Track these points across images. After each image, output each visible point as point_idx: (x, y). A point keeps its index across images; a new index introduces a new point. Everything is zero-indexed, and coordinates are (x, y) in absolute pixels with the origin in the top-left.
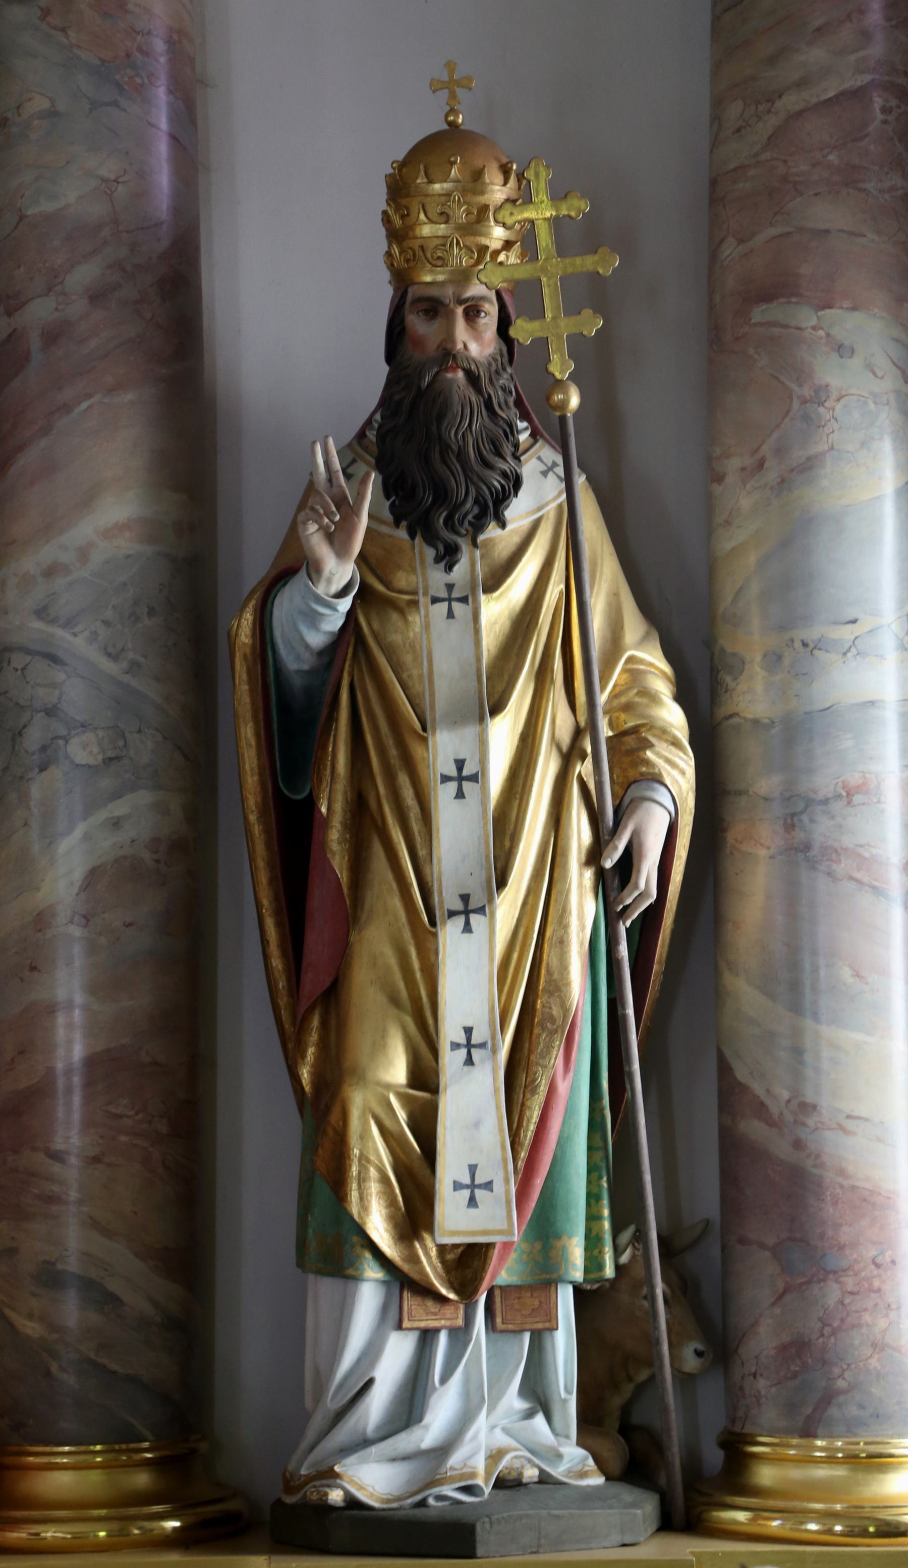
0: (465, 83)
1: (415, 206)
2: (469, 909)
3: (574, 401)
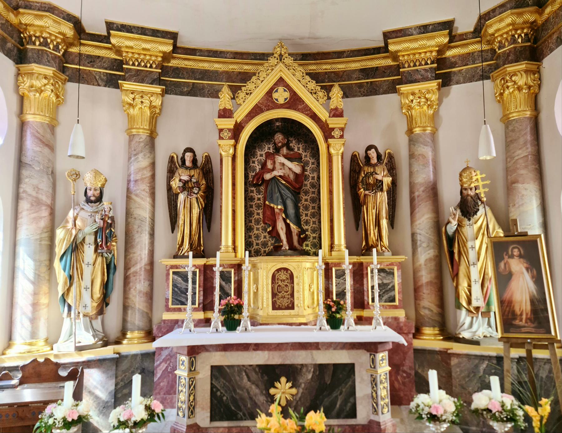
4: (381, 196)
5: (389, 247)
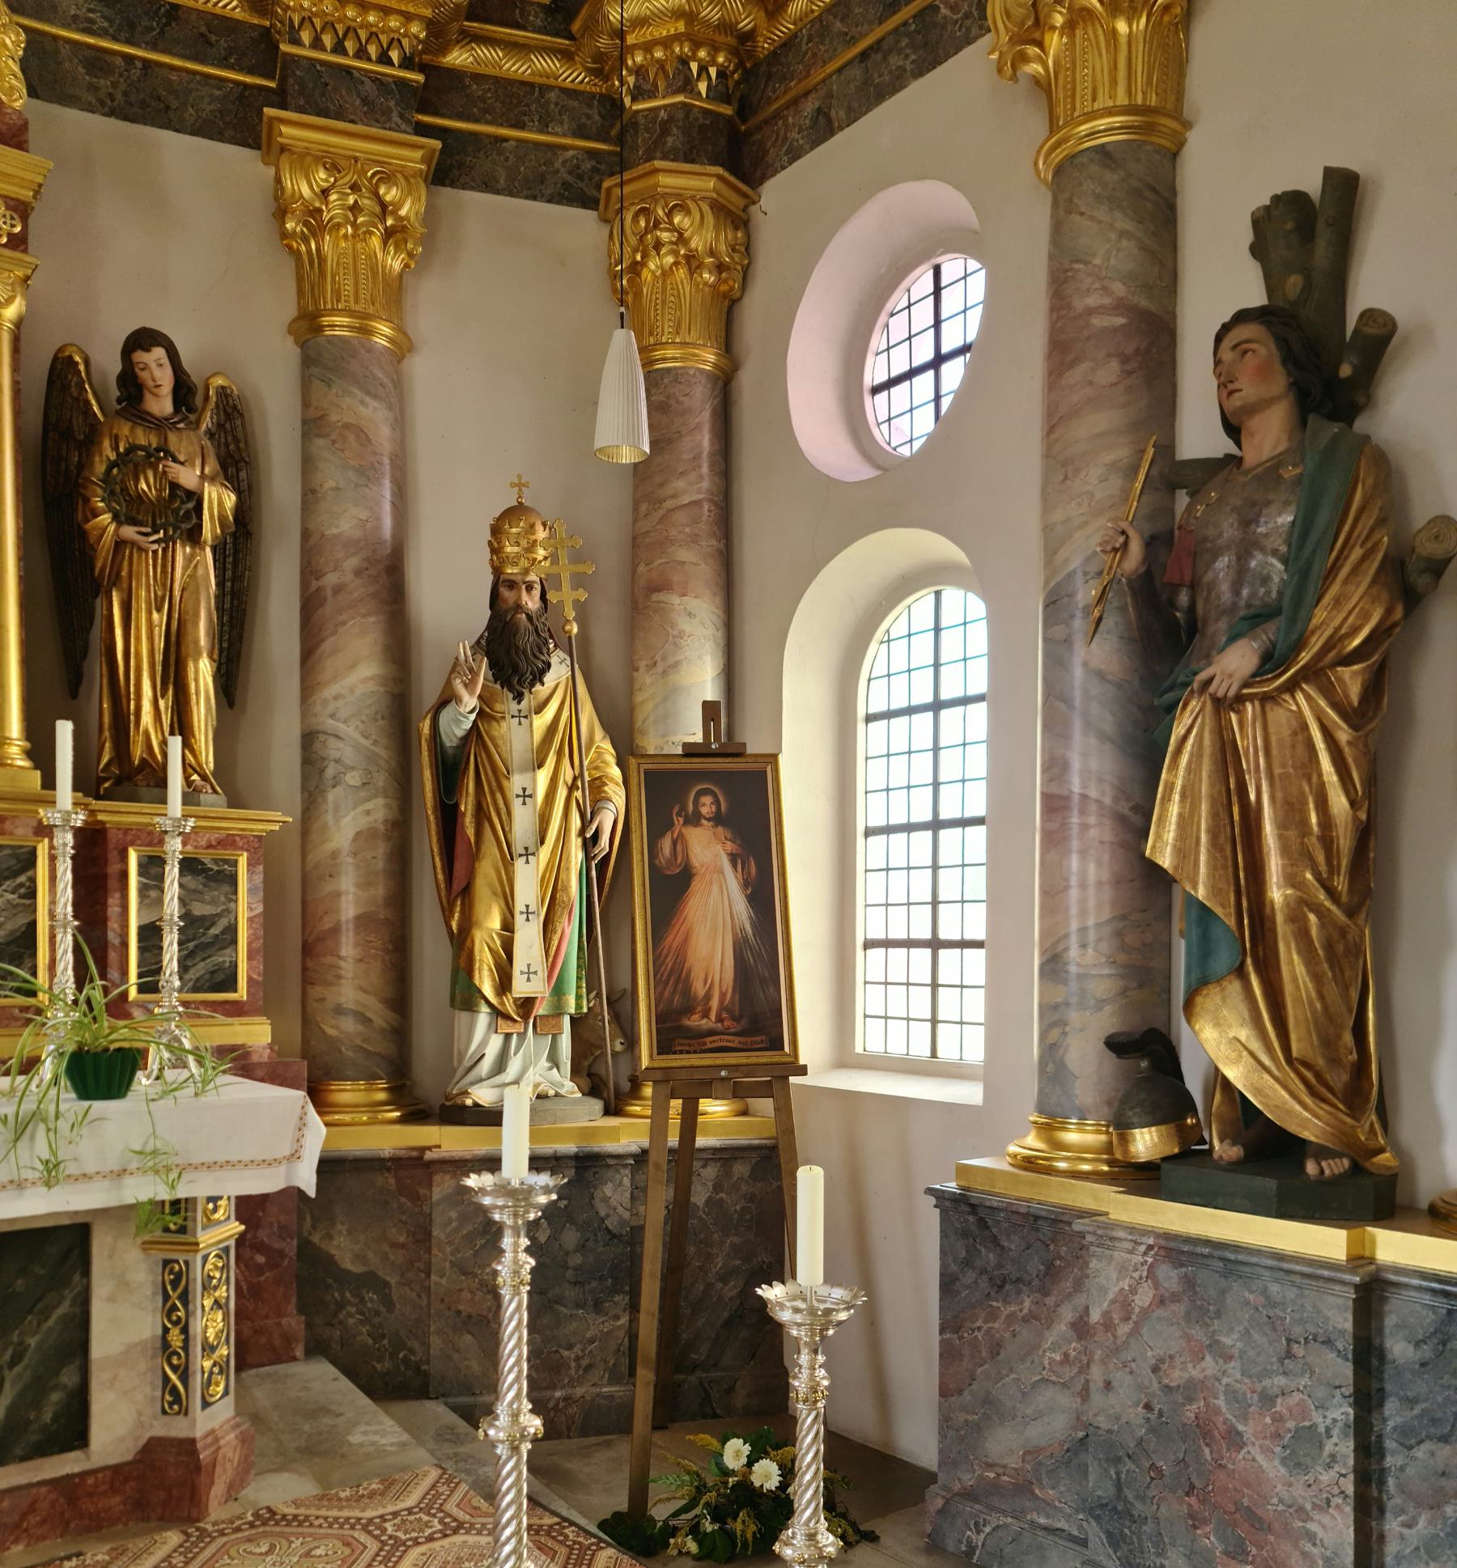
0: (526, 485)
1: (504, 538)
2: (527, 853)
3: (575, 630)
4: (189, 560)
5: (214, 774)
